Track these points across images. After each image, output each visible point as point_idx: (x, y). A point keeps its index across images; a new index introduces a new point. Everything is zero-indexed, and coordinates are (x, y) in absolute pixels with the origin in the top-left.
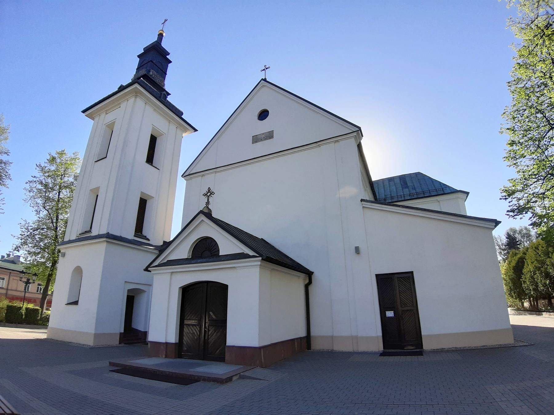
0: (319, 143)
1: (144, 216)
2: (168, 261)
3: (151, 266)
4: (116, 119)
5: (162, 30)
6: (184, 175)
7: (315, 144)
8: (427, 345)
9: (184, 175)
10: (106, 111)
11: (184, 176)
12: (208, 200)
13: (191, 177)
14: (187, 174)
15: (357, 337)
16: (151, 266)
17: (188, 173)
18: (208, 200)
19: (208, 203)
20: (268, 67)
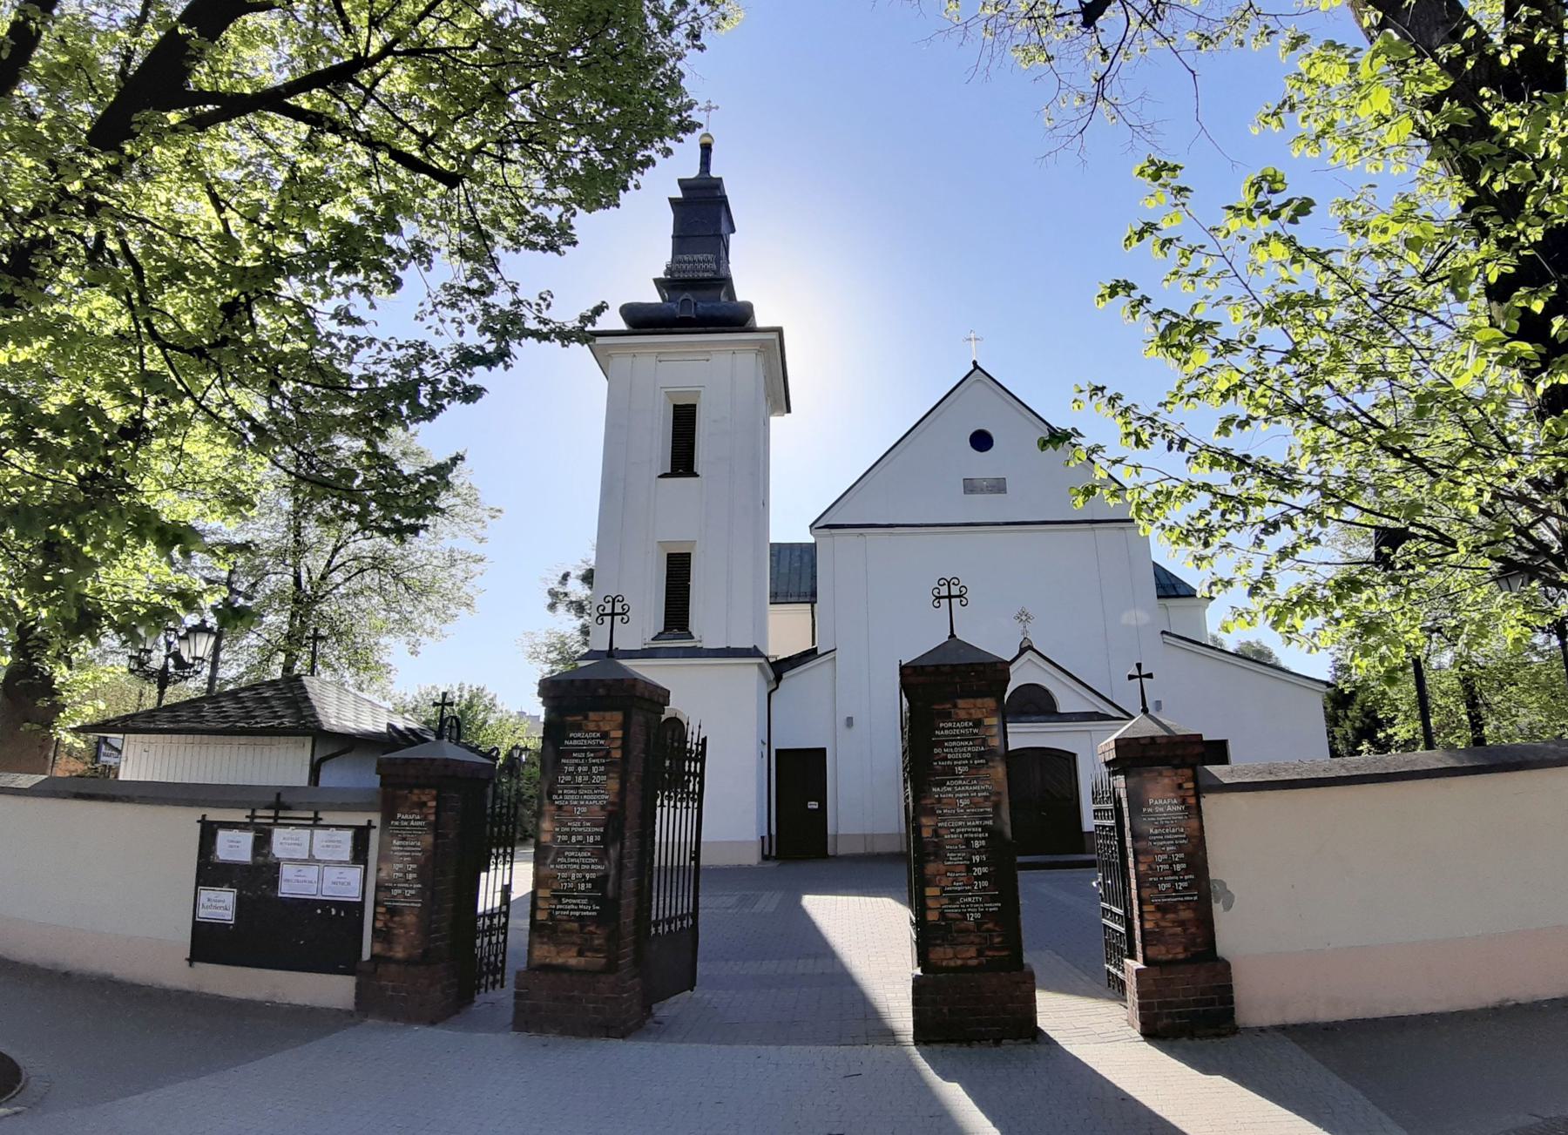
19: (1025, 632)
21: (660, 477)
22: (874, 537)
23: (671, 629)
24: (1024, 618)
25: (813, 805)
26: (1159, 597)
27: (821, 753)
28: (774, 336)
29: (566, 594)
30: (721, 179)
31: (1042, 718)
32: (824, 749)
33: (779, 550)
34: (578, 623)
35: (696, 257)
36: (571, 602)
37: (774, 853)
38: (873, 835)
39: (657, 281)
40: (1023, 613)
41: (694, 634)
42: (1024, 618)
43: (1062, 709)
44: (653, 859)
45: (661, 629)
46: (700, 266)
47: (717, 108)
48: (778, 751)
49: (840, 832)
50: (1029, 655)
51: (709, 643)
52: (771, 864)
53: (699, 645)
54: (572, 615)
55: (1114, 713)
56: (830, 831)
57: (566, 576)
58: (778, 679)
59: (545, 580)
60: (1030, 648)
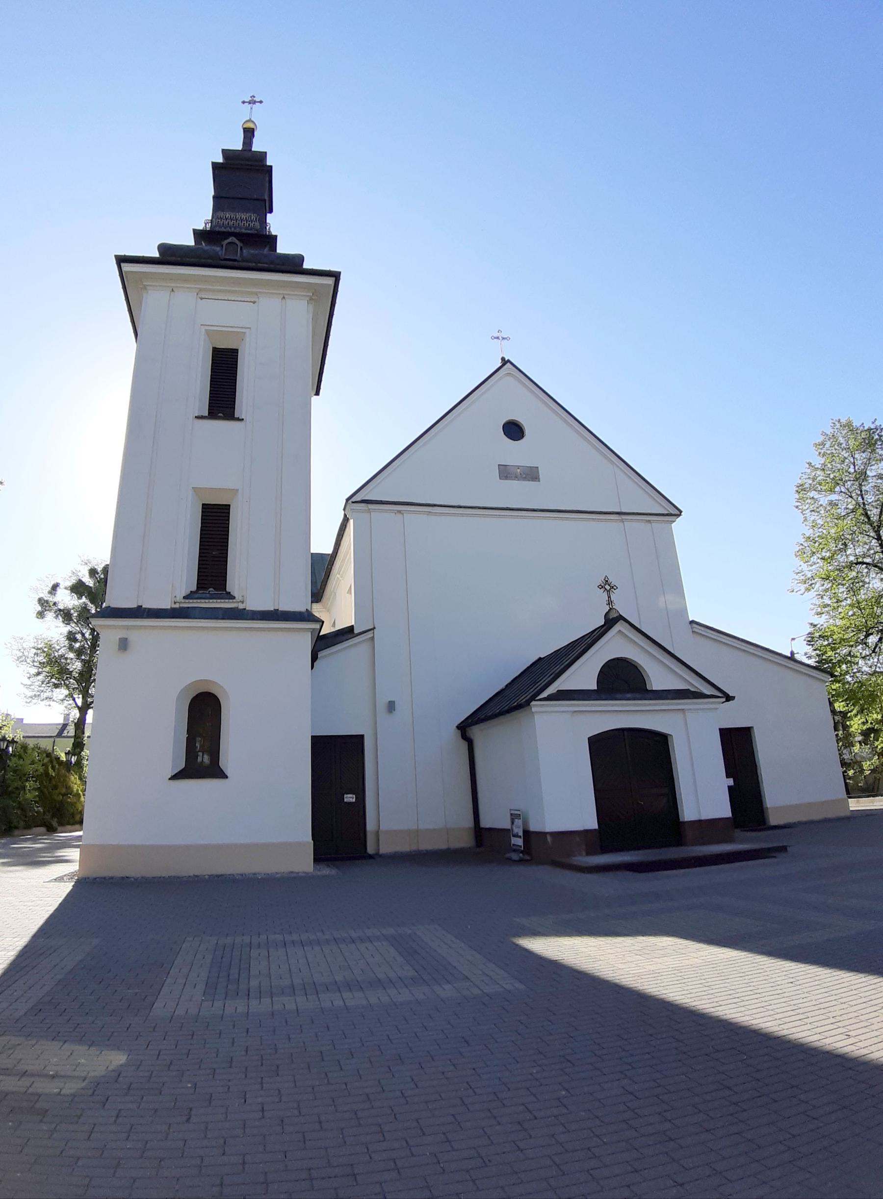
0: (624, 517)
1: (226, 561)
2: (558, 691)
4: (250, 328)
5: (250, 121)
6: (353, 499)
7: (617, 516)
8: (773, 820)
9: (353, 499)
10: (200, 290)
11: (353, 502)
12: (609, 597)
13: (370, 507)
14: (357, 500)
15: (417, 831)
17: (363, 496)
18: (609, 597)
19: (610, 602)
20: (495, 340)
21: (196, 417)
22: (414, 519)
23: (206, 589)
24: (608, 587)
25: (350, 798)
27: (359, 740)
28: (330, 281)
29: (55, 604)
30: (266, 153)
31: (637, 695)
32: (362, 737)
33: (313, 555)
34: (65, 629)
35: (238, 216)
36: (60, 610)
39: (195, 231)
41: (235, 593)
42: (608, 587)
44: (61, 833)
45: (194, 588)
46: (243, 220)
47: (261, 102)
50: (619, 626)
51: (253, 604)
52: (326, 871)
53: (241, 606)
54: (59, 622)
55: (707, 690)
56: (370, 826)
57: (55, 587)
59: (36, 590)
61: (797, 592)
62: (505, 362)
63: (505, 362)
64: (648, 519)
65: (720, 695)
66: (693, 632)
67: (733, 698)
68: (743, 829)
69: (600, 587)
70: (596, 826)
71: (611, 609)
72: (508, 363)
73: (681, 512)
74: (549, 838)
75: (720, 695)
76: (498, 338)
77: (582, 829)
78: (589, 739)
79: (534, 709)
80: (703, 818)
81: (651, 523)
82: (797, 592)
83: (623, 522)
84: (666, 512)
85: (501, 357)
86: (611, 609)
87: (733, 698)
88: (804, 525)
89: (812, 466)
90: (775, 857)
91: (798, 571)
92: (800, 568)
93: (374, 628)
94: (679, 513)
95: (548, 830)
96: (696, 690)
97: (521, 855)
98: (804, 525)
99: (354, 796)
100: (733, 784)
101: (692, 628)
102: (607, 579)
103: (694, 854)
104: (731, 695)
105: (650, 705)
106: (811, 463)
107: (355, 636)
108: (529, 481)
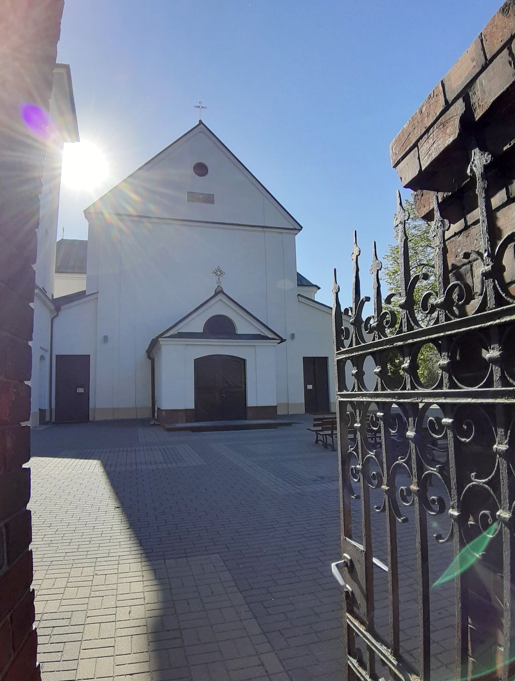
2: (178, 333)
3: (163, 336)
7: (261, 228)
16: (163, 336)
19: (219, 282)
24: (219, 273)
26: (298, 285)
37: (53, 419)
38: (118, 409)
40: (219, 270)
42: (219, 273)
43: (239, 331)
48: (57, 356)
49: (97, 407)
50: (220, 296)
56: (91, 406)
58: (58, 309)
60: (222, 292)
61: (383, 280)
62: (201, 122)
63: (201, 122)
64: (280, 231)
65: (277, 338)
66: (299, 301)
67: (285, 340)
68: (311, 413)
69: (214, 273)
70: (194, 408)
71: (218, 286)
72: (201, 125)
73: (302, 228)
74: (164, 413)
75: (277, 338)
76: (199, 107)
77: (184, 409)
78: (244, 361)
79: (161, 343)
80: (258, 406)
81: (282, 234)
82: (383, 280)
83: (282, 234)
84: (293, 228)
85: (199, 120)
86: (218, 286)
87: (285, 340)
88: (396, 239)
89: (409, 202)
90: (276, 428)
91: (385, 267)
92: (387, 266)
93: (98, 292)
94: (301, 229)
95: (163, 409)
96: (263, 335)
97: (156, 422)
98: (396, 239)
99: (83, 389)
100: (312, 388)
101: (298, 299)
102: (219, 268)
103: (206, 422)
104: (284, 338)
105: (190, 341)
106: (407, 200)
107: (85, 297)
108: (207, 203)
